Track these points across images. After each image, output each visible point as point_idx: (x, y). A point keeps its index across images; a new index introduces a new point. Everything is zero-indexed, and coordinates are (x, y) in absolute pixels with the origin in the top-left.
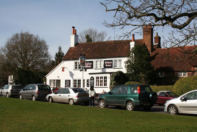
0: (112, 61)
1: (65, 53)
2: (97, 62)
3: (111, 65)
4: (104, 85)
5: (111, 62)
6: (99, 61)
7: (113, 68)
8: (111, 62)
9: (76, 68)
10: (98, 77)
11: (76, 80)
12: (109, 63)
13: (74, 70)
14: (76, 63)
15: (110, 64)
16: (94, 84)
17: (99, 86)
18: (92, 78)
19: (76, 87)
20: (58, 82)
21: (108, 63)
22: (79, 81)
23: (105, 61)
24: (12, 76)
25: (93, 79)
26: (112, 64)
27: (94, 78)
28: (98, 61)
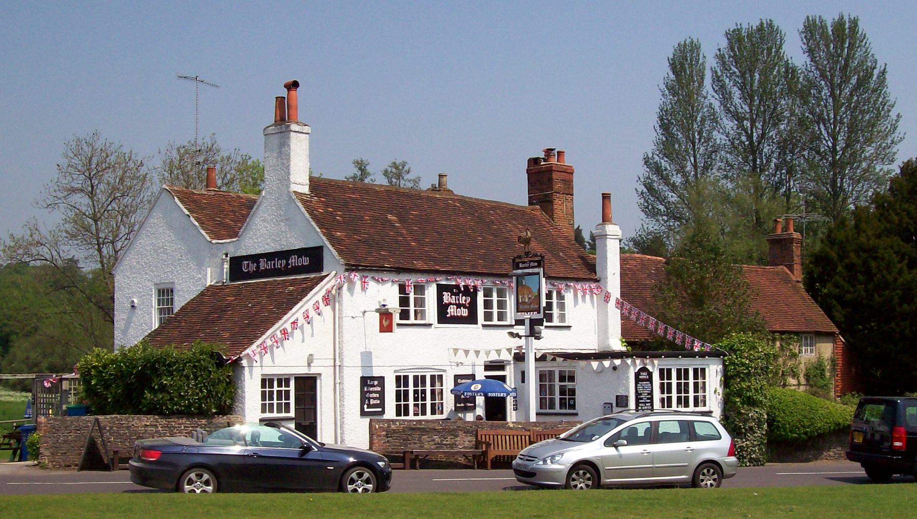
4: (696, 404)
10: (551, 373)
14: (402, 289)
15: (376, 392)
16: (651, 399)
17: (557, 409)
19: (424, 413)
22: (420, 380)
25: (650, 380)
27: (650, 374)
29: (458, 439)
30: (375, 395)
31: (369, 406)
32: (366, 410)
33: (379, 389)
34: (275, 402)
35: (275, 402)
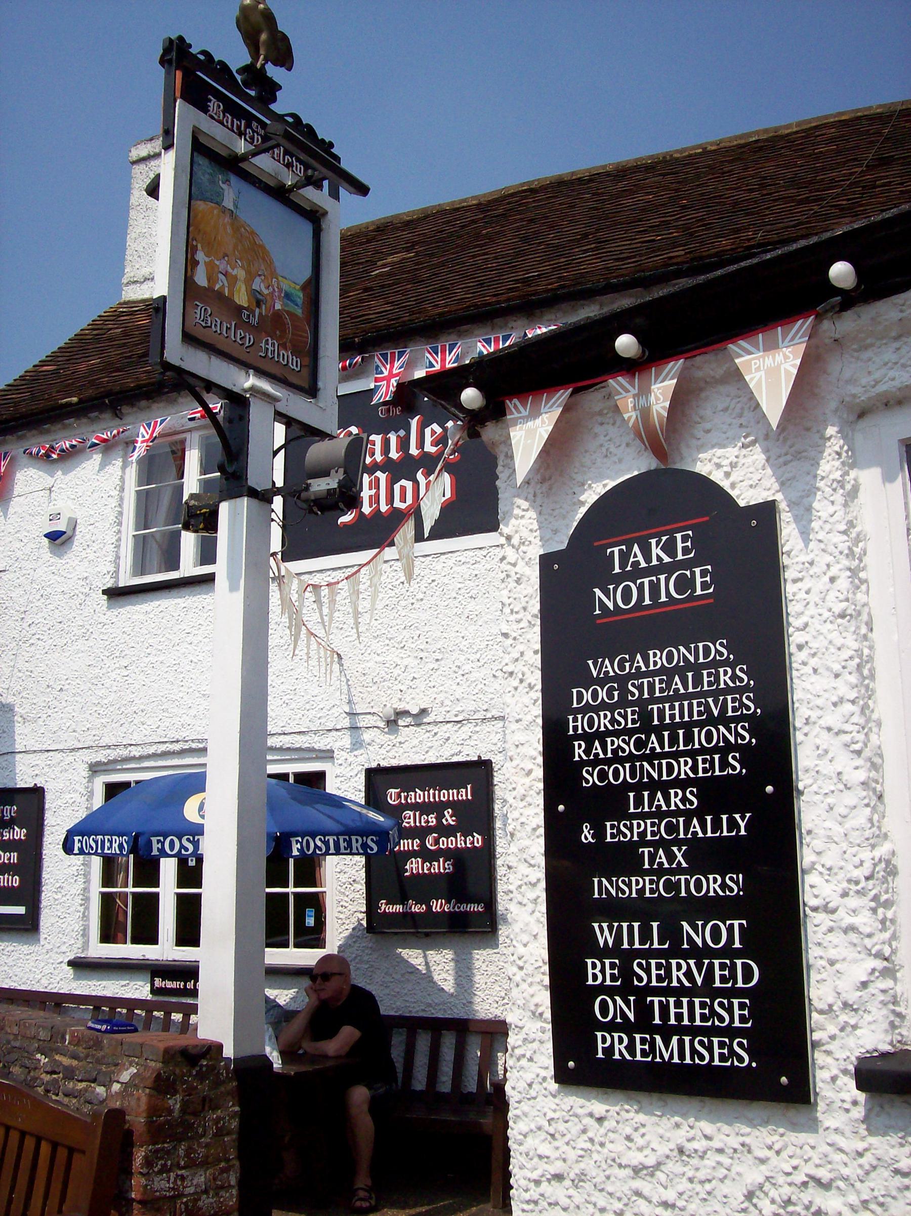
13: (116, 594)
18: (657, 570)
19: (146, 933)
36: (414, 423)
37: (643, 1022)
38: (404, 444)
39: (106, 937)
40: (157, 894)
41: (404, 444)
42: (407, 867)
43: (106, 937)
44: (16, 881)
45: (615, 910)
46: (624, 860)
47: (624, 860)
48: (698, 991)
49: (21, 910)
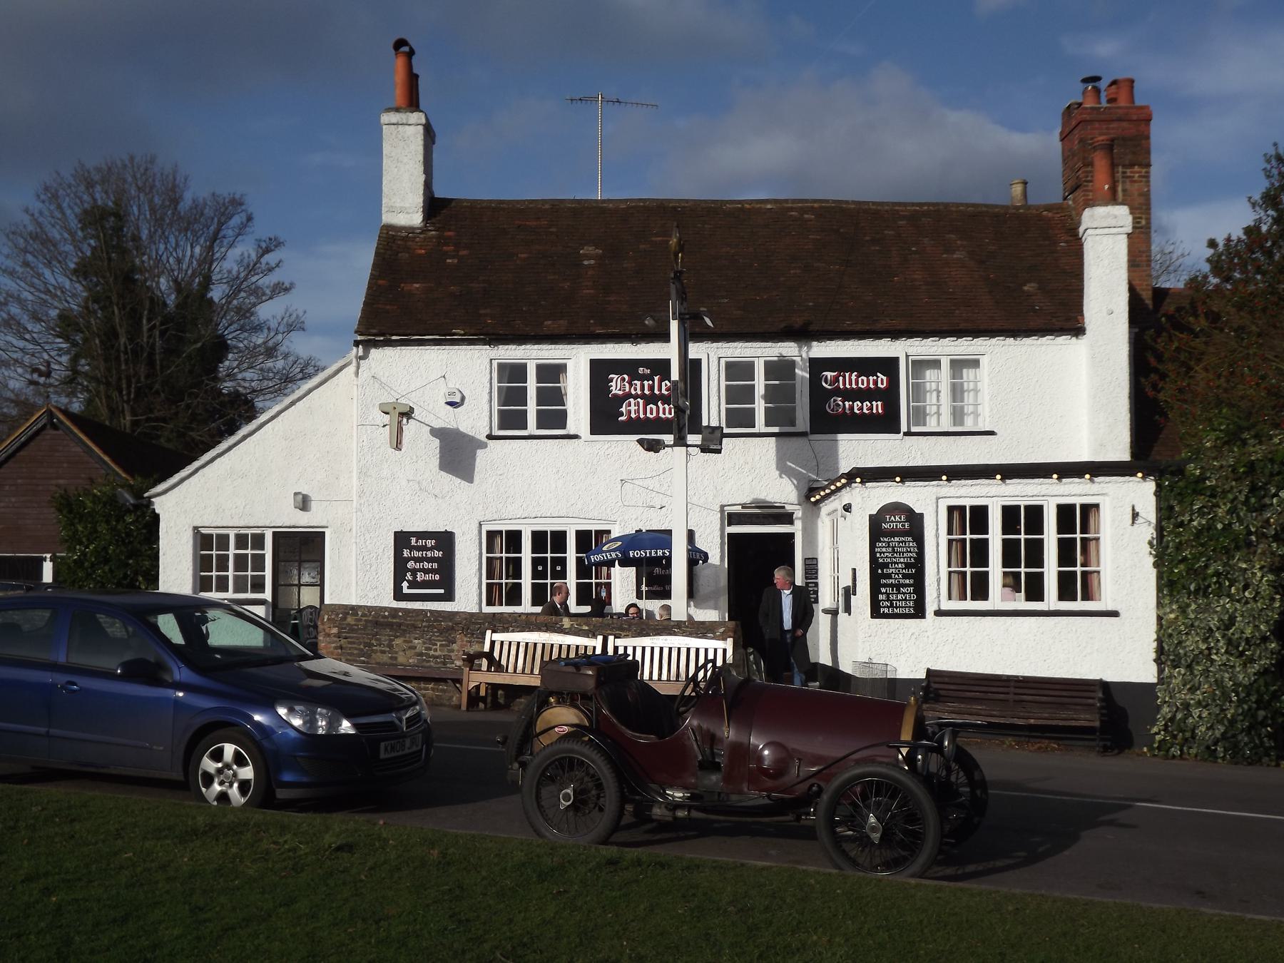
0: (889, 366)
1: (183, 642)
2: (738, 371)
3: (878, 407)
5: (882, 381)
6: (945, 363)
7: (904, 428)
8: (882, 381)
9: (733, 519)
11: (514, 539)
12: (864, 382)
14: (514, 372)
15: (430, 560)
20: (302, 549)
21: (852, 380)
22: (549, 541)
23: (817, 366)
24: (482, 312)
26: (890, 396)
28: (936, 364)
29: (455, 646)
30: (426, 565)
31: (413, 585)
32: (406, 591)
33: (438, 554)
34: (231, 573)
35: (231, 573)
36: (656, 378)
37: (892, 605)
38: (651, 388)
39: (489, 603)
40: (1042, 573)
41: (651, 388)
42: (623, 409)
43: (489, 603)
44: (437, 577)
45: (885, 586)
46: (889, 576)
47: (889, 576)
48: (904, 598)
49: (442, 591)
